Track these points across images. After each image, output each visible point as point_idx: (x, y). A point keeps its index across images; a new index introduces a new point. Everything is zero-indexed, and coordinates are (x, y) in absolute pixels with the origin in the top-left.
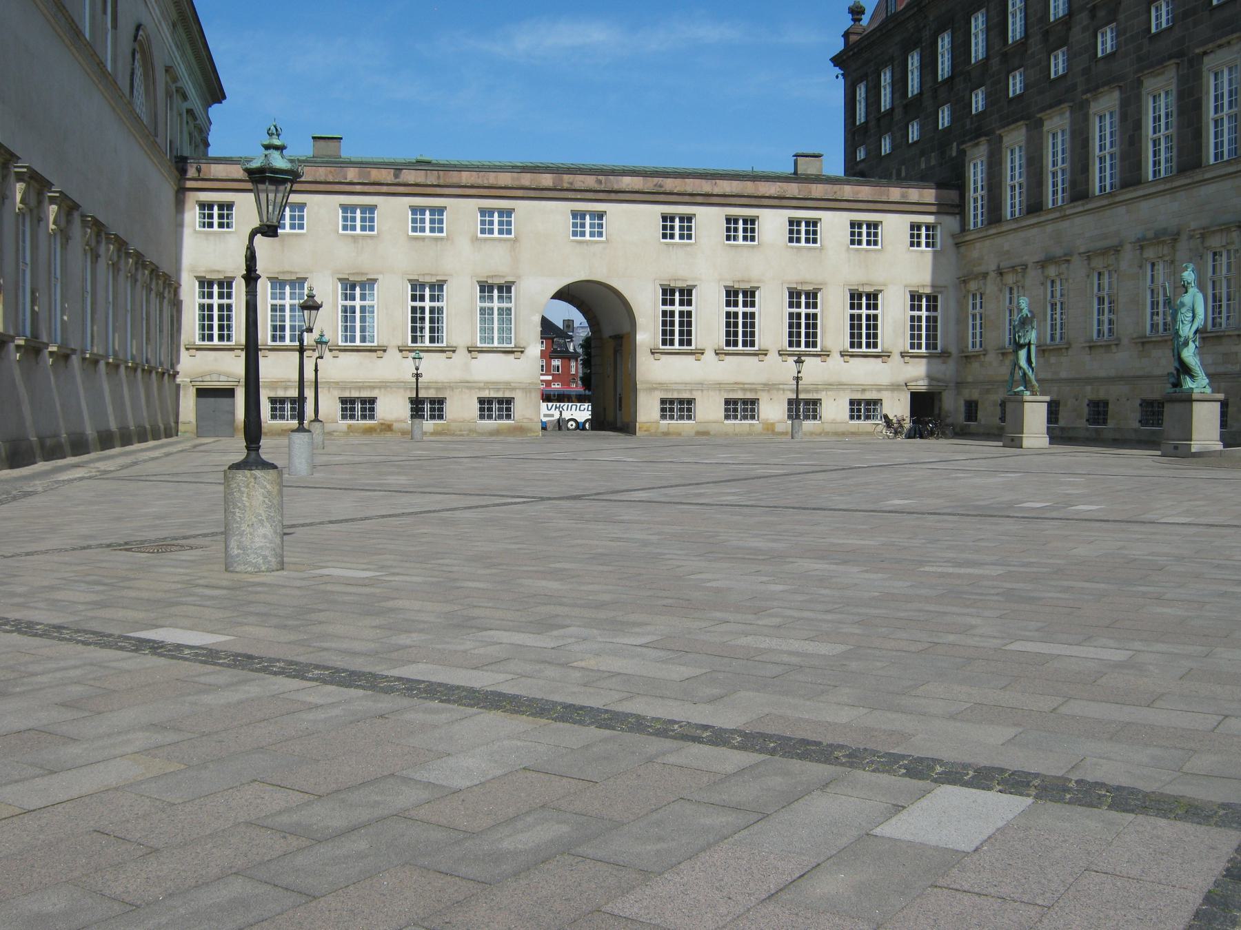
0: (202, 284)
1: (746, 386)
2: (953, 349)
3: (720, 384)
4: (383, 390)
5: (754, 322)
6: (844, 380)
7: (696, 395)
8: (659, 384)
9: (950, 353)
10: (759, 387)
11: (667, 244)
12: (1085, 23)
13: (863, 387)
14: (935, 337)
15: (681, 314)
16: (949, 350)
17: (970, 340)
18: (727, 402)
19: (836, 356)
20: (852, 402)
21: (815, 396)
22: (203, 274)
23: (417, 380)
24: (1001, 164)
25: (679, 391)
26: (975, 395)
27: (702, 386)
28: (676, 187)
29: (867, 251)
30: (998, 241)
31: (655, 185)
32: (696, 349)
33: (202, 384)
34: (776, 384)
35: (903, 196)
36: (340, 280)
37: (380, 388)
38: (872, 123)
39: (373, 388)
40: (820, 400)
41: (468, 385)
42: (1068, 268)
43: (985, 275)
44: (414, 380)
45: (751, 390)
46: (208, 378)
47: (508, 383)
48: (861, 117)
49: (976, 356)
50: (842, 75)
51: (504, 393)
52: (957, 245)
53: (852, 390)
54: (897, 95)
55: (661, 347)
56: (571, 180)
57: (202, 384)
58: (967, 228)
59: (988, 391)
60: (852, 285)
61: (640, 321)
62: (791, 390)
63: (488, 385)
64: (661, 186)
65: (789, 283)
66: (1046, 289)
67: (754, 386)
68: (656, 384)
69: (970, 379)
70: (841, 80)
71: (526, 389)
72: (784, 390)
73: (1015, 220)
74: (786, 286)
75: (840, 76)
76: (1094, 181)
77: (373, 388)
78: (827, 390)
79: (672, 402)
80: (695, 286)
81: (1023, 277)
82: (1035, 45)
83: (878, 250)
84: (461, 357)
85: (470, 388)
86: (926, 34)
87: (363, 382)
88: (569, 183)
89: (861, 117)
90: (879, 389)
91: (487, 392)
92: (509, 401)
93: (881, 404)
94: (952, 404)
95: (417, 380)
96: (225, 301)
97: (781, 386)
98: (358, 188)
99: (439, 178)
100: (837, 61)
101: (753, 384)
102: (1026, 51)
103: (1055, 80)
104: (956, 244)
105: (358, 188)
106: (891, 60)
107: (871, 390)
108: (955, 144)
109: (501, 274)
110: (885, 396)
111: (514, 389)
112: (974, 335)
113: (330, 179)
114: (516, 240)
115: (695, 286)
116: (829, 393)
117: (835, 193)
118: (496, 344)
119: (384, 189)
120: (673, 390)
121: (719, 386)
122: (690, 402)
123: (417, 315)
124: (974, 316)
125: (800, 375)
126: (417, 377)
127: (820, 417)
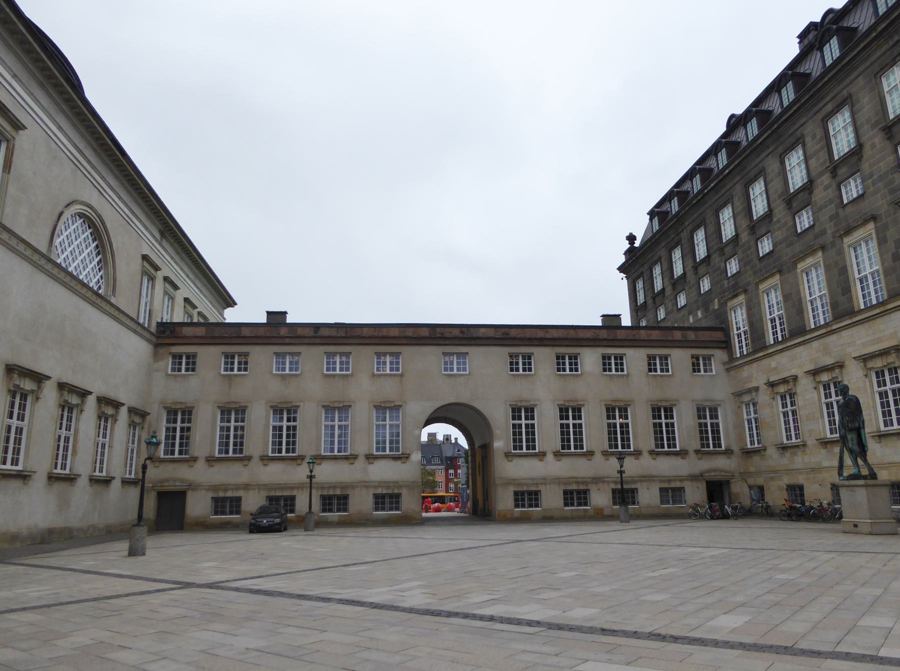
0: (169, 413)
1: (579, 480)
2: (735, 448)
3: (558, 479)
4: (300, 490)
5: (581, 415)
6: (654, 473)
7: (541, 488)
8: (513, 480)
9: (732, 450)
10: (589, 480)
11: (513, 375)
12: (826, 183)
13: (668, 478)
14: (719, 439)
15: (527, 426)
16: (731, 449)
17: (748, 440)
18: (565, 492)
19: (646, 455)
20: (661, 490)
21: (633, 486)
22: (169, 405)
23: (621, 475)
24: (760, 305)
25: (527, 485)
26: (760, 481)
27: (545, 481)
28: (518, 334)
29: (661, 376)
30: (765, 362)
31: (503, 334)
32: (540, 452)
33: (162, 488)
34: (602, 478)
35: (683, 336)
36: (219, 407)
37: (298, 488)
38: (650, 301)
39: (292, 488)
40: (637, 489)
41: (365, 485)
42: (841, 373)
43: (757, 389)
44: (619, 475)
45: (583, 483)
46: (166, 484)
47: (397, 482)
48: (641, 299)
49: (756, 452)
50: (626, 277)
51: (393, 490)
52: (728, 370)
53: (661, 481)
54: (666, 280)
55: (513, 451)
56: (442, 332)
57: (162, 488)
58: (734, 357)
59: (772, 478)
60: (653, 401)
61: (497, 432)
62: (615, 483)
63: (382, 484)
64: (507, 334)
65: (605, 401)
66: (819, 394)
67: (585, 480)
68: (509, 480)
69: (752, 469)
70: (625, 280)
71: (410, 486)
72: (608, 482)
73: (776, 342)
74: (603, 403)
75: (624, 278)
76: (857, 298)
77: (292, 488)
78: (641, 481)
79: (523, 493)
80: (536, 405)
81: (795, 385)
82: (780, 212)
83: (669, 375)
84: (360, 463)
85: (366, 487)
86: (684, 235)
87: (286, 484)
88: (440, 333)
89: (641, 299)
90: (681, 479)
91: (380, 489)
92: (398, 496)
93: (684, 491)
94: (741, 492)
95: (621, 475)
96: (292, 424)
97: (606, 479)
98: (287, 341)
99: (347, 332)
100: (621, 269)
101: (585, 478)
102: (772, 220)
103: (801, 233)
104: (727, 369)
105: (287, 341)
106: (659, 260)
107: (675, 480)
108: (716, 300)
109: (391, 400)
110: (404, 492)
111: (401, 487)
112: (751, 436)
113: (268, 334)
114: (402, 375)
115: (536, 405)
116: (644, 484)
117: (634, 335)
118: (388, 452)
119: (306, 341)
120: (523, 484)
121: (557, 481)
122: (537, 493)
123: (702, 428)
124: (749, 422)
125: (622, 469)
126: (621, 473)
127: (638, 503)
